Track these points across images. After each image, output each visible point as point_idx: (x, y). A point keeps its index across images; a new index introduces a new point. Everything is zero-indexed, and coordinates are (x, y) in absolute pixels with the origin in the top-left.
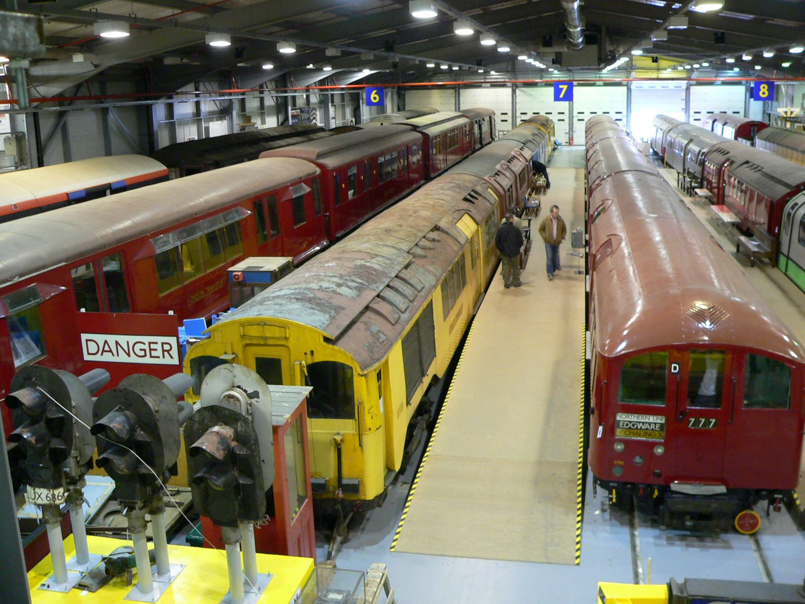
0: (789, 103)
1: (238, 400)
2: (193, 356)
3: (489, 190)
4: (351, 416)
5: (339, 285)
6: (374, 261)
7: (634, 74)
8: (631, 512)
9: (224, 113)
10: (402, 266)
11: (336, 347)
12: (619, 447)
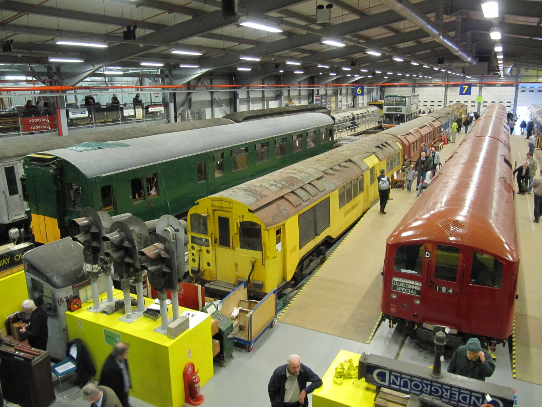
1: (169, 232)
2: (191, 213)
3: (398, 143)
4: (261, 250)
5: (272, 185)
6: (300, 175)
9: (278, 97)
11: (253, 215)
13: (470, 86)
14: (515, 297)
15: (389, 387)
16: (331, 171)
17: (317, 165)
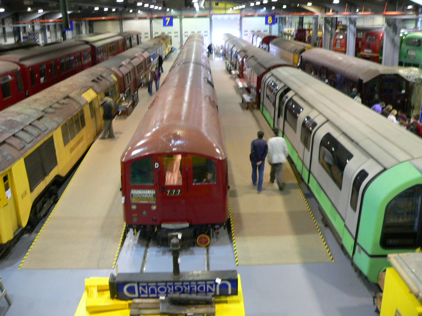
0: (289, 26)
6: (19, 117)
7: (212, 12)
8: (149, 241)
10: (36, 118)
12: (134, 207)
13: (172, 18)
14: (227, 188)
15: (139, 297)
16: (50, 110)
17: (36, 105)
